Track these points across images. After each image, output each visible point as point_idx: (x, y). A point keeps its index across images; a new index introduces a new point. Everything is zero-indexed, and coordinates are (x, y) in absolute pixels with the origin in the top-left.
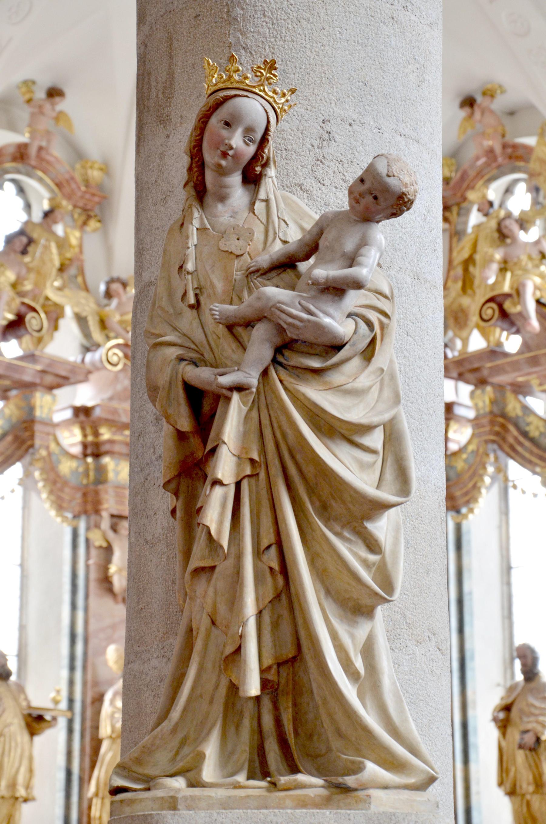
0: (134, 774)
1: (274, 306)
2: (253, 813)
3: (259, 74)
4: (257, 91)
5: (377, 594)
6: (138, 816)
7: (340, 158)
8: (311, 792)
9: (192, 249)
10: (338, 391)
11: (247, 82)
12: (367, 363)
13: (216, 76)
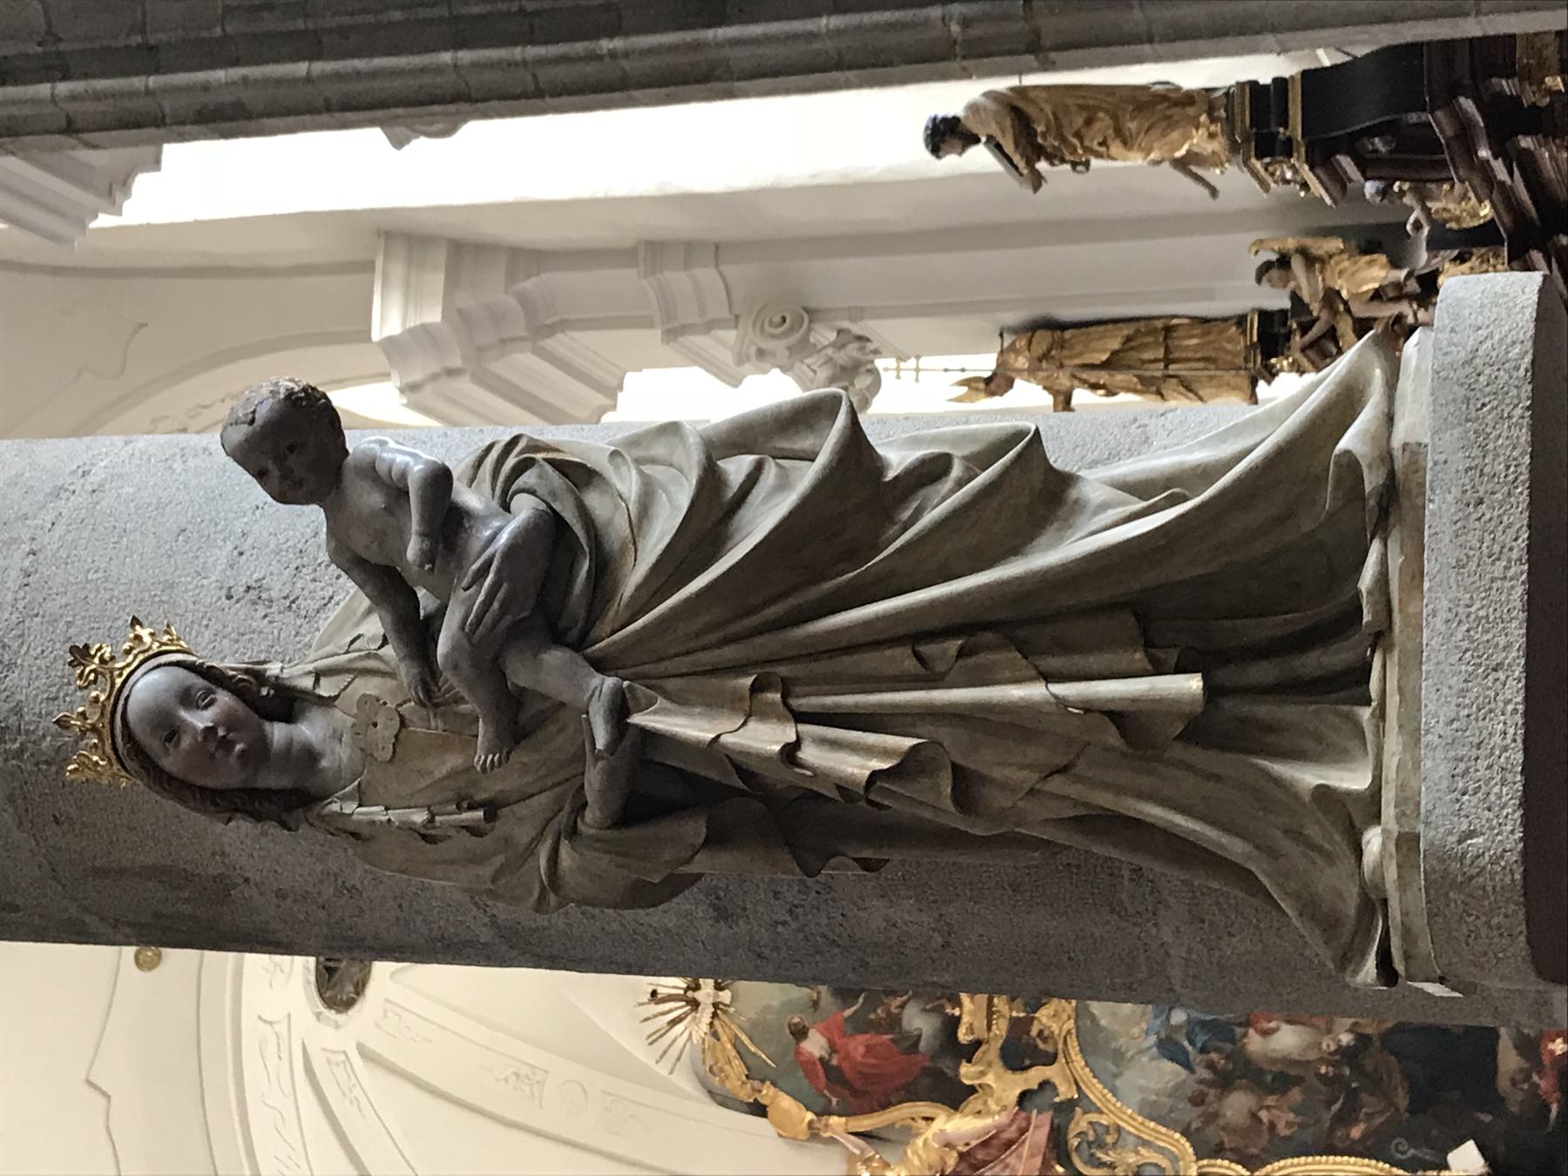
0: (1357, 940)
1: (469, 637)
2: (1429, 659)
3: (92, 677)
4: (119, 681)
5: (1020, 455)
6: (1428, 902)
7: (291, 570)
8: (1396, 561)
9: (392, 815)
10: (640, 528)
11: (103, 698)
12: (596, 480)
13: (95, 758)
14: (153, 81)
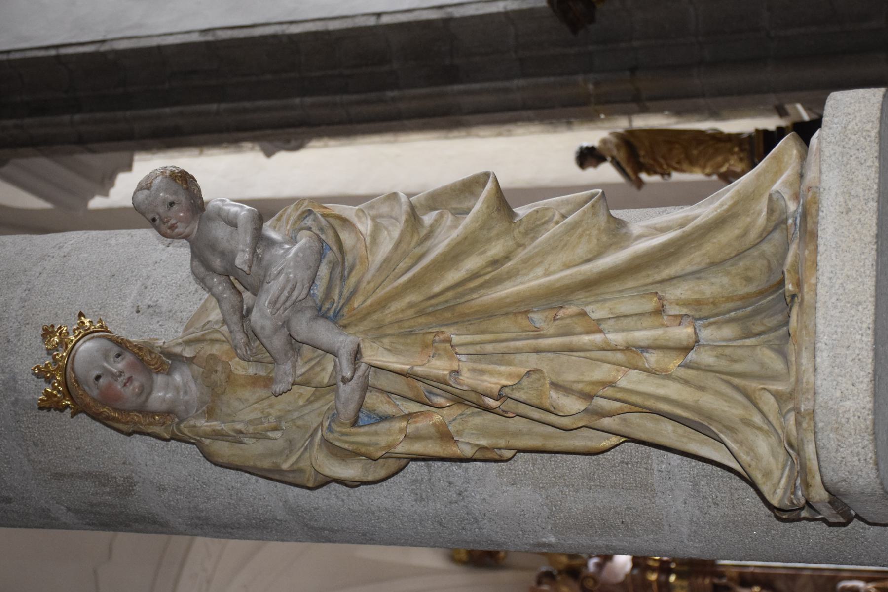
4: (70, 346)
14: (128, 114)
